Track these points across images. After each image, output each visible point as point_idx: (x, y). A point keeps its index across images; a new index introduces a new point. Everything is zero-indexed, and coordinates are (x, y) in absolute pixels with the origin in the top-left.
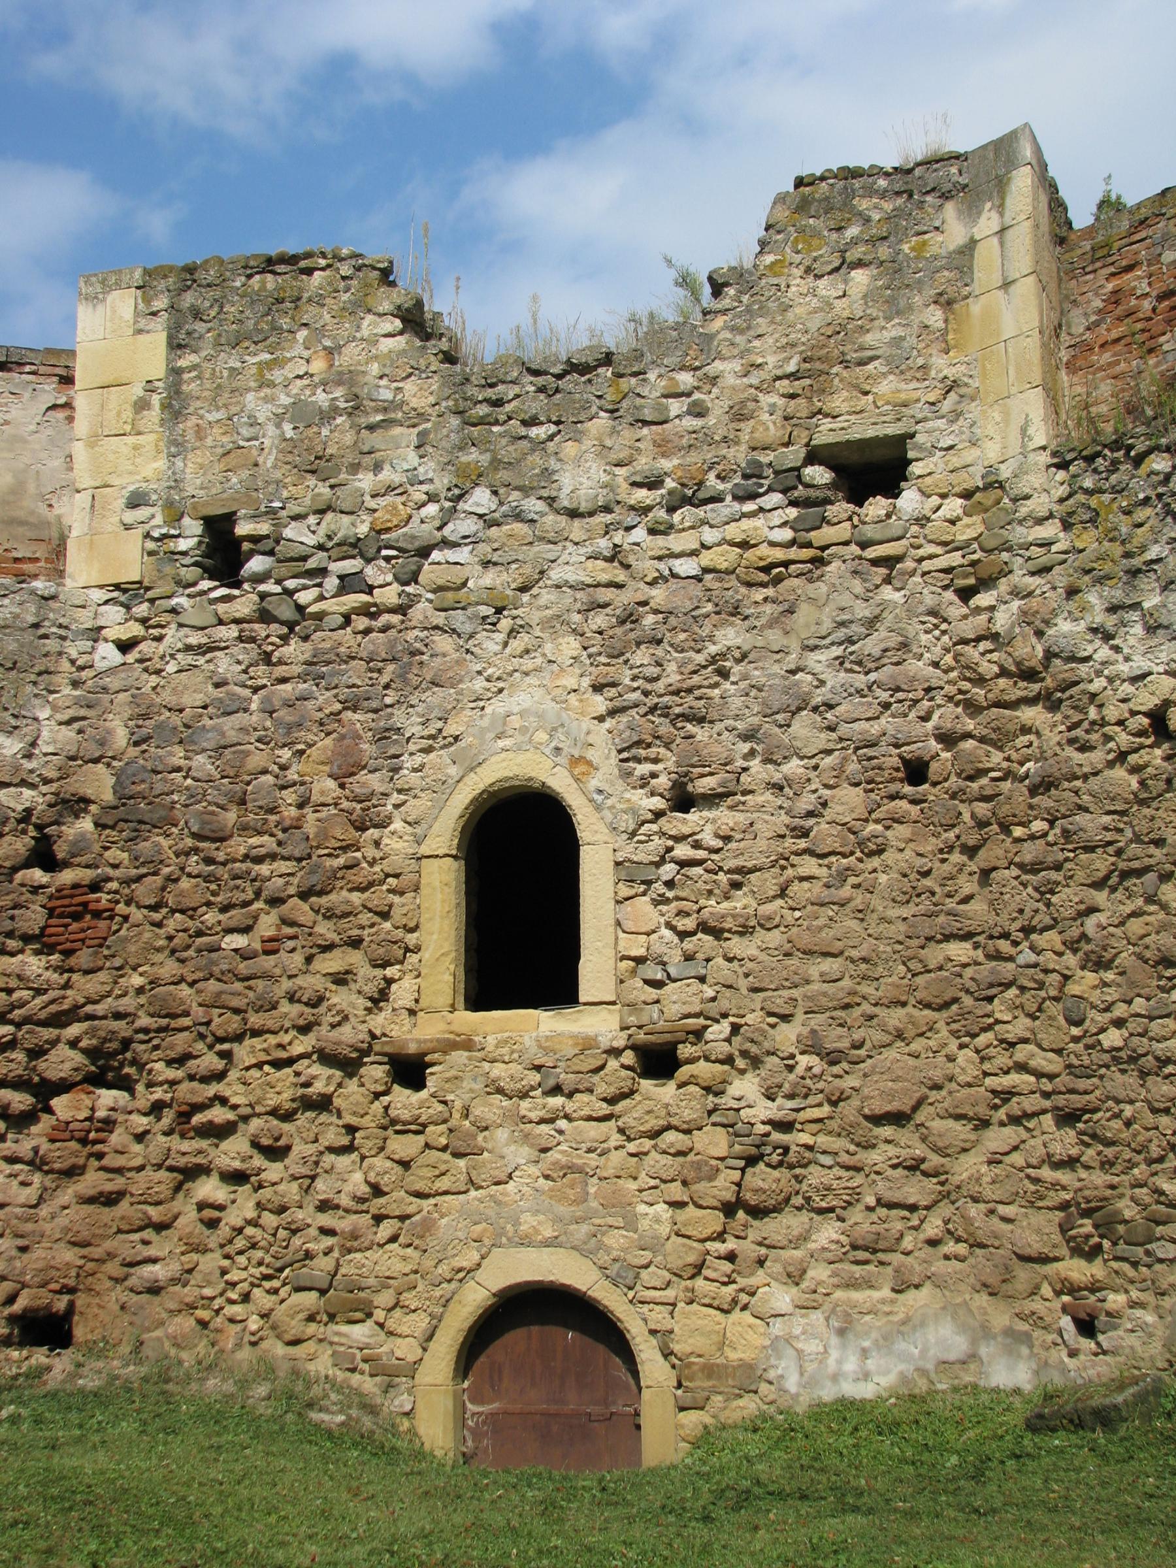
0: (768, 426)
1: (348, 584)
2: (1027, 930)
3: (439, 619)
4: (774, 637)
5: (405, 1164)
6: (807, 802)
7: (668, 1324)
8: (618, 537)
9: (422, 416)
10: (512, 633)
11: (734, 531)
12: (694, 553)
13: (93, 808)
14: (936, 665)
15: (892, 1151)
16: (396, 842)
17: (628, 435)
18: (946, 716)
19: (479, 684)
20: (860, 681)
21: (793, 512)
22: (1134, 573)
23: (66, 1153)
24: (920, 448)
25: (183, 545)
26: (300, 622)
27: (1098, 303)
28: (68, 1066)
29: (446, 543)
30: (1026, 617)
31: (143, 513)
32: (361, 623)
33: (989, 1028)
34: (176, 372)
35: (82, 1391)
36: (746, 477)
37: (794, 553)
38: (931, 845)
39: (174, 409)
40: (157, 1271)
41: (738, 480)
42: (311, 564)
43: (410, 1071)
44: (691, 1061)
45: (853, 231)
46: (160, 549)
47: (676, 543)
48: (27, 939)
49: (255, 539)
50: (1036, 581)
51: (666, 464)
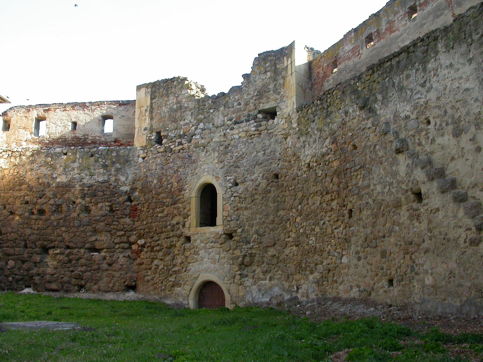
0: (251, 106)
1: (180, 144)
13: (138, 190)
21: (255, 124)
23: (134, 256)
28: (134, 239)
31: (146, 131)
32: (182, 151)
34: (151, 104)
35: (164, 304)
36: (247, 117)
40: (149, 278)
42: (173, 140)
44: (235, 236)
48: (126, 215)
49: (164, 136)
51: (234, 116)
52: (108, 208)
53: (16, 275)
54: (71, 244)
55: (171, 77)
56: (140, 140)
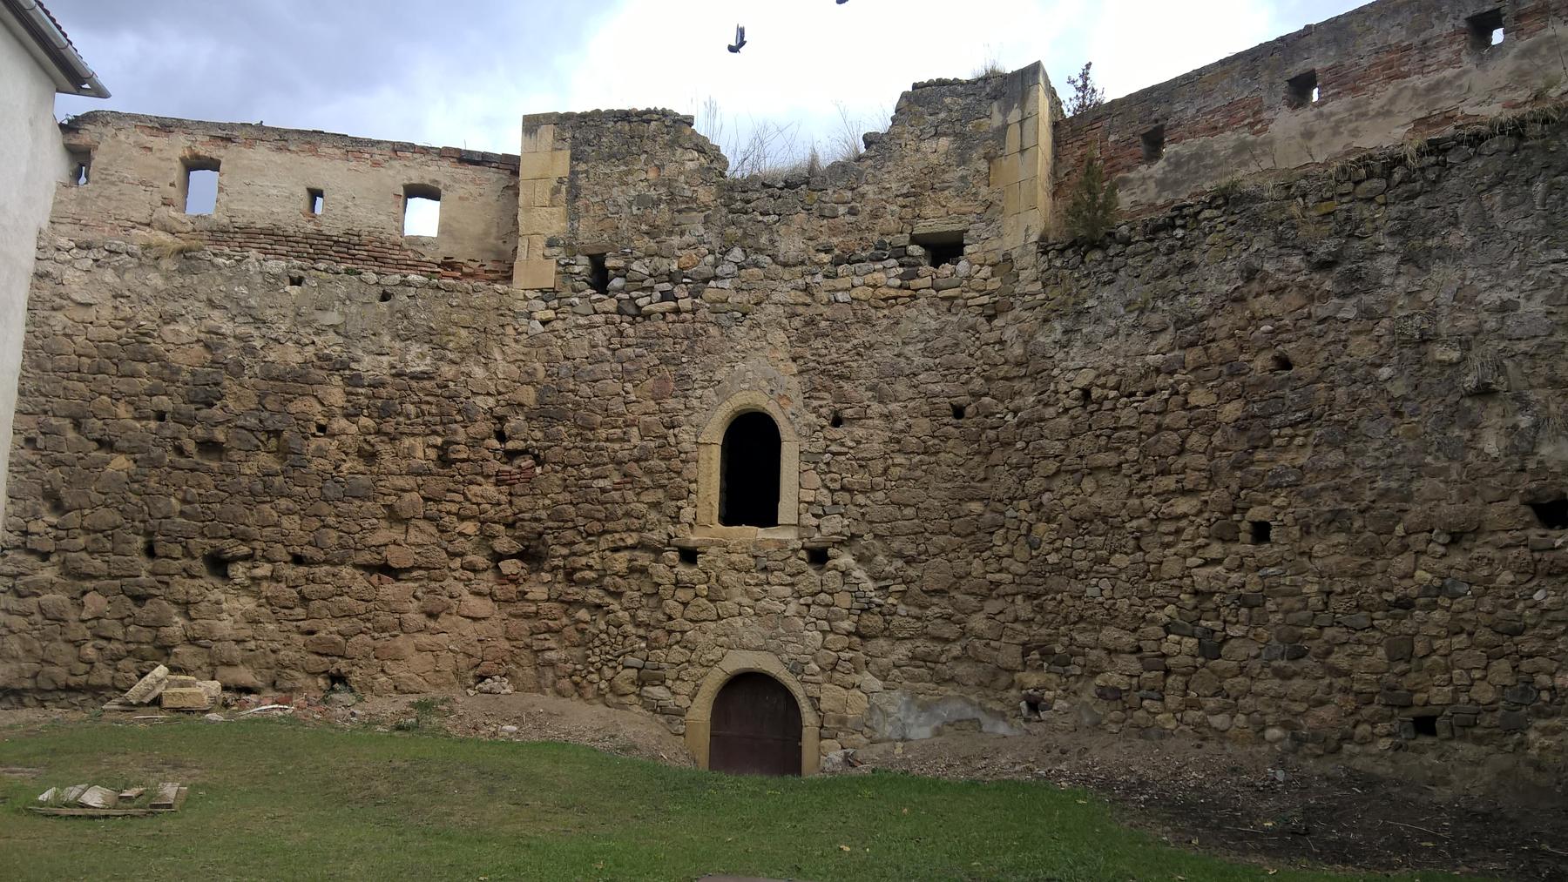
0: (889, 222)
1: (665, 296)
2: (1012, 499)
3: (712, 318)
4: (889, 338)
5: (685, 604)
6: (900, 425)
7: (817, 694)
8: (808, 279)
9: (707, 207)
10: (751, 328)
11: (869, 279)
12: (847, 290)
14: (971, 355)
15: (937, 610)
16: (686, 436)
17: (816, 223)
18: (977, 384)
19: (731, 355)
20: (931, 362)
21: (901, 270)
22: (1080, 313)
24: (970, 238)
25: (577, 269)
26: (641, 315)
27: (1072, 161)
29: (716, 278)
30: (1020, 334)
31: (556, 250)
32: (671, 317)
33: (990, 548)
34: (573, 173)
37: (900, 293)
38: (965, 450)
39: (574, 194)
41: (872, 250)
42: (646, 284)
43: (689, 556)
45: (942, 115)
46: (565, 272)
47: (839, 283)
48: (488, 476)
49: (616, 269)
50: (1027, 314)
51: (835, 241)
52: (432, 454)
53: (109, 639)
54: (309, 552)
55: (641, 107)
56: (536, 269)
